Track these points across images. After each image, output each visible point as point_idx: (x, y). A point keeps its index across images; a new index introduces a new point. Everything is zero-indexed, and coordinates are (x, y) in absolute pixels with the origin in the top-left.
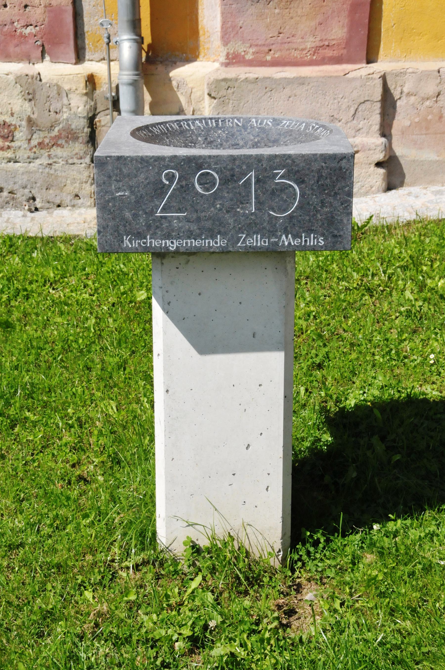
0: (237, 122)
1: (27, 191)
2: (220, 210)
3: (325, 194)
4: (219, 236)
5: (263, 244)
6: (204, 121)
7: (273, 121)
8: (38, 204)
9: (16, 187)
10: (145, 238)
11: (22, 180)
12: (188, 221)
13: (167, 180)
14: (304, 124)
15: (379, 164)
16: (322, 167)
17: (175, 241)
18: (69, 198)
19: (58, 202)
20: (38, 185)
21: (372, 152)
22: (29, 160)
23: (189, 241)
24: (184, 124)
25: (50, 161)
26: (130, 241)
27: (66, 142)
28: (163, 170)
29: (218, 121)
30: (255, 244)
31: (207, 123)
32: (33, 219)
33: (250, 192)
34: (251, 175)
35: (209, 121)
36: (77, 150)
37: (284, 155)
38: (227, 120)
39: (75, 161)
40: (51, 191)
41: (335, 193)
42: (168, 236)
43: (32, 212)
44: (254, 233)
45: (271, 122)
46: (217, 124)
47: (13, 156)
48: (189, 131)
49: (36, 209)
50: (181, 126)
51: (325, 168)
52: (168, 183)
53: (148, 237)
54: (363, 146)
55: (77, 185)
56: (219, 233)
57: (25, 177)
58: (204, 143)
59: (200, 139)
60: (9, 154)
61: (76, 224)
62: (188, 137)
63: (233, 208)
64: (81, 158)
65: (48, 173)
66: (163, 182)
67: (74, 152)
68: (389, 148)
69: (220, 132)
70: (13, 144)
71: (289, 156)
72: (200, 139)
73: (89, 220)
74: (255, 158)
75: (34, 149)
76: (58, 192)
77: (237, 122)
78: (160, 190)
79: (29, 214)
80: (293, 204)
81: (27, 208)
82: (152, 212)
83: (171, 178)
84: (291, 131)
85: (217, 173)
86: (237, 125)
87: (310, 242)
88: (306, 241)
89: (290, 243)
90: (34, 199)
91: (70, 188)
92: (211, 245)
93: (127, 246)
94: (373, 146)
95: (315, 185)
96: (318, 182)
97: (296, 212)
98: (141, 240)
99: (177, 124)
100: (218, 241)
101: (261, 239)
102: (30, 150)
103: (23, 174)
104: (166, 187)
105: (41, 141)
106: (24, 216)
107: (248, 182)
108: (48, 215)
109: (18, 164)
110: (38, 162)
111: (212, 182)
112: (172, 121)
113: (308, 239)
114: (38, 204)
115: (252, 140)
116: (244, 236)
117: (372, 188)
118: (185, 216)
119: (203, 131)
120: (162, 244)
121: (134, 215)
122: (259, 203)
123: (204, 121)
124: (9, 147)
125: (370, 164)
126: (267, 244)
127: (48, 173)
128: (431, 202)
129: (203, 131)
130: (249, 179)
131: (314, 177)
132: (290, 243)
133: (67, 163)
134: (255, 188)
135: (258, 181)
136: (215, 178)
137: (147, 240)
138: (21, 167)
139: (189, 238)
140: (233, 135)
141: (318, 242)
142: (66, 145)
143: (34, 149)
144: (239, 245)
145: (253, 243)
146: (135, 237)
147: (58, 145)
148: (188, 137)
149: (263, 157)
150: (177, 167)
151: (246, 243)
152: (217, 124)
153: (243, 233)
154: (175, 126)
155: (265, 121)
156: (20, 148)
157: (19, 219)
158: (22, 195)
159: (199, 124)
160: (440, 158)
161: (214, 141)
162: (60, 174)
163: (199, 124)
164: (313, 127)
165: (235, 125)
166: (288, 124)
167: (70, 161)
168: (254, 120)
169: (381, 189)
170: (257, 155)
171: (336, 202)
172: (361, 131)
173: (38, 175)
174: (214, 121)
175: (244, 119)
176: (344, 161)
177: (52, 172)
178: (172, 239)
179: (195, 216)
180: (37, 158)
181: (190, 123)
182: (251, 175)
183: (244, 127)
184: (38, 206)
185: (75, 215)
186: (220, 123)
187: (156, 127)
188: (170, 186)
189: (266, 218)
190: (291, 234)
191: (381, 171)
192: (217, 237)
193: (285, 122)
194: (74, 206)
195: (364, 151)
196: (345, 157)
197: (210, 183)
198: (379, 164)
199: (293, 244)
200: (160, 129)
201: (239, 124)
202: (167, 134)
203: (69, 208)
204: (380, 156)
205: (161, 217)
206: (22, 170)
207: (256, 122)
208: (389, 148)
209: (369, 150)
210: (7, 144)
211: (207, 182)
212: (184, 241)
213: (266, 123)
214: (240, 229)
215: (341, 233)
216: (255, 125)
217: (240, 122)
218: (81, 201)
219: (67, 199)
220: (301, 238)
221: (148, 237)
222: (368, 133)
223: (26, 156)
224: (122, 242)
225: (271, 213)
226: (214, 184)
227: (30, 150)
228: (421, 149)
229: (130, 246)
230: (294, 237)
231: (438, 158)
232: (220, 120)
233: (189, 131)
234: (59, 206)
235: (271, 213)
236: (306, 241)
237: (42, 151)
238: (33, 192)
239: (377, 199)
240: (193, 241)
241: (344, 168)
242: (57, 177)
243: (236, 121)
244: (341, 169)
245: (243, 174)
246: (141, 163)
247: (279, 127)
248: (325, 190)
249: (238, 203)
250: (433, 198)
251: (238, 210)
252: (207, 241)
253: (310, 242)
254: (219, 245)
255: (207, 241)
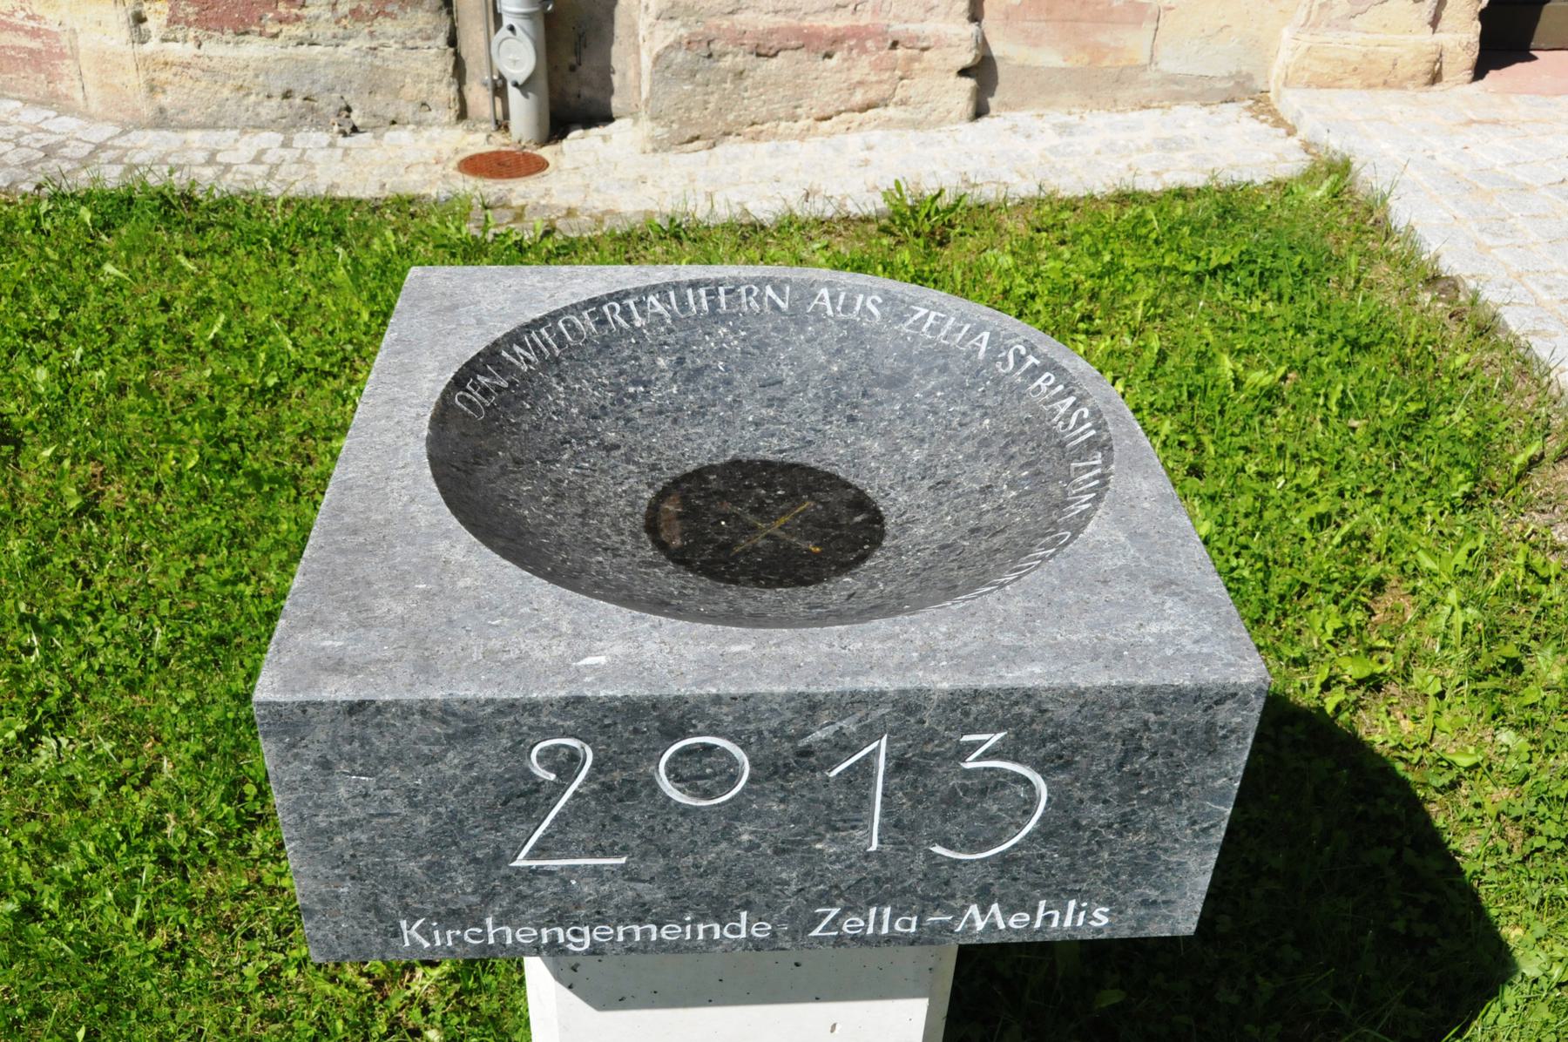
0: (774, 296)
1: (335, 96)
2: (753, 846)
3: (1141, 798)
4: (744, 915)
5: (898, 927)
6: (672, 294)
7: (885, 301)
8: (356, 118)
9: (316, 89)
10: (480, 923)
11: (327, 76)
12: (631, 880)
13: (549, 769)
14: (986, 335)
15: (964, 72)
16: (1146, 723)
17: (586, 930)
18: (411, 108)
19: (392, 116)
20: (355, 85)
21: (953, 50)
22: (335, 41)
23: (637, 929)
24: (612, 309)
25: (373, 44)
26: (426, 932)
27: (401, 8)
28: (531, 741)
29: (716, 293)
30: (870, 931)
31: (682, 301)
32: (346, 151)
33: (867, 798)
34: (875, 752)
35: (690, 291)
36: (420, 25)
37: (1010, 692)
38: (743, 290)
39: (419, 43)
40: (378, 98)
41: (1177, 795)
42: (560, 917)
43: (345, 134)
44: (870, 904)
45: (878, 306)
46: (714, 305)
47: (307, 33)
48: (628, 335)
49: (355, 129)
50: (603, 322)
51: (1155, 728)
52: (552, 777)
53: (489, 921)
54: (939, 39)
55: (424, 86)
56: (747, 905)
57: (331, 72)
58: (674, 380)
59: (662, 362)
60: (299, 30)
61: (421, 168)
62: (625, 361)
63: (800, 843)
64: (429, 38)
65: (371, 65)
66: (533, 776)
67: (416, 28)
68: (983, 44)
69: (722, 331)
70: (305, 12)
71: (1028, 695)
72: (662, 362)
73: (445, 157)
74: (895, 703)
75: (344, 22)
76: (390, 98)
77: (774, 296)
78: (526, 798)
79: (341, 140)
80: (1020, 827)
81: (336, 128)
82: (498, 858)
83: (566, 765)
84: (945, 352)
85: (744, 747)
86: (776, 307)
87: (1061, 921)
88: (1048, 918)
89: (992, 926)
90: (349, 109)
91: (410, 91)
92: (717, 936)
93: (415, 945)
94: (955, 40)
95: (1109, 774)
96: (1121, 765)
97: (1028, 849)
98: (463, 929)
99: (592, 314)
100: (743, 925)
101: (893, 917)
102: (337, 22)
103: (326, 65)
104: (545, 791)
105: (354, 6)
106: (331, 145)
107: (865, 769)
108: (373, 142)
109: (317, 48)
110: (352, 44)
111: (723, 772)
112: (574, 306)
113: (1056, 914)
114: (356, 118)
115: (821, 368)
116: (835, 911)
117: (949, 112)
118: (622, 867)
119: (670, 331)
120: (540, 937)
121: (430, 866)
122: (895, 824)
123: (672, 294)
124: (298, 18)
125: (949, 71)
126: (913, 929)
127: (371, 65)
128: (1053, 150)
129: (670, 331)
130: (868, 764)
131: (1110, 751)
132: (992, 926)
133: (405, 48)
134: (885, 788)
135: (899, 765)
136: (733, 762)
137: (485, 928)
138: (324, 54)
139: (639, 920)
140: (761, 346)
141: (1089, 917)
142: (400, 15)
143: (344, 22)
144: (816, 933)
145: (865, 928)
146: (439, 921)
147: (387, 15)
148: (625, 361)
149: (927, 698)
150: (586, 729)
151: (840, 929)
152: (714, 305)
153: (832, 905)
154: (586, 323)
155: (860, 298)
156: (318, 18)
157: (322, 153)
158: (328, 105)
159: (660, 308)
160: (1069, 64)
161: (708, 366)
162: (392, 67)
163: (660, 308)
164: (1020, 360)
165: (767, 309)
166: (930, 320)
167: (410, 43)
168: (824, 292)
169: (965, 117)
170: (904, 692)
171: (1175, 817)
172: (935, 11)
173: (353, 68)
174: (702, 292)
175: (796, 287)
176: (1229, 704)
177: (378, 62)
178: (576, 923)
179: (658, 865)
180: (350, 38)
181: (633, 307)
182: (875, 752)
183: (797, 317)
184: (358, 123)
185: (422, 143)
186: (723, 299)
187: (522, 345)
188: (559, 788)
189: (919, 864)
190: (1000, 902)
191: (969, 83)
192: (738, 915)
193: (923, 311)
194: (419, 123)
195: (940, 48)
196: (1234, 695)
197: (715, 774)
198: (964, 72)
199: (1002, 926)
200: (535, 347)
201: (779, 302)
202: (557, 361)
203: (411, 127)
204: (967, 59)
205: (535, 872)
206: (324, 59)
207: (831, 298)
208: (983, 44)
209: (949, 46)
210: (295, 11)
211: (699, 770)
212: (621, 929)
213: (864, 307)
214: (822, 895)
215: (1173, 896)
216: (830, 312)
217: (781, 294)
218: (433, 113)
219: (408, 111)
220: (1033, 911)
221: (489, 921)
222: (947, 14)
223: (329, 34)
224: (397, 933)
225: (938, 849)
226: (733, 780)
227: (337, 22)
228: (1036, 45)
229: (427, 945)
230: (1008, 911)
231: (1063, 65)
232: (721, 290)
233: (628, 335)
234: (394, 123)
235: (938, 849)
236: (1048, 918)
237: (359, 25)
238: (347, 97)
239: (959, 136)
240: (654, 928)
241: (1222, 728)
242: (387, 71)
243: (769, 291)
244: (1210, 727)
245: (845, 748)
246: (443, 721)
247: (904, 328)
248: (1142, 787)
249: (821, 829)
250: (1056, 141)
251: (819, 846)
252: (701, 927)
253: (1061, 921)
254: (743, 935)
255: (701, 927)
